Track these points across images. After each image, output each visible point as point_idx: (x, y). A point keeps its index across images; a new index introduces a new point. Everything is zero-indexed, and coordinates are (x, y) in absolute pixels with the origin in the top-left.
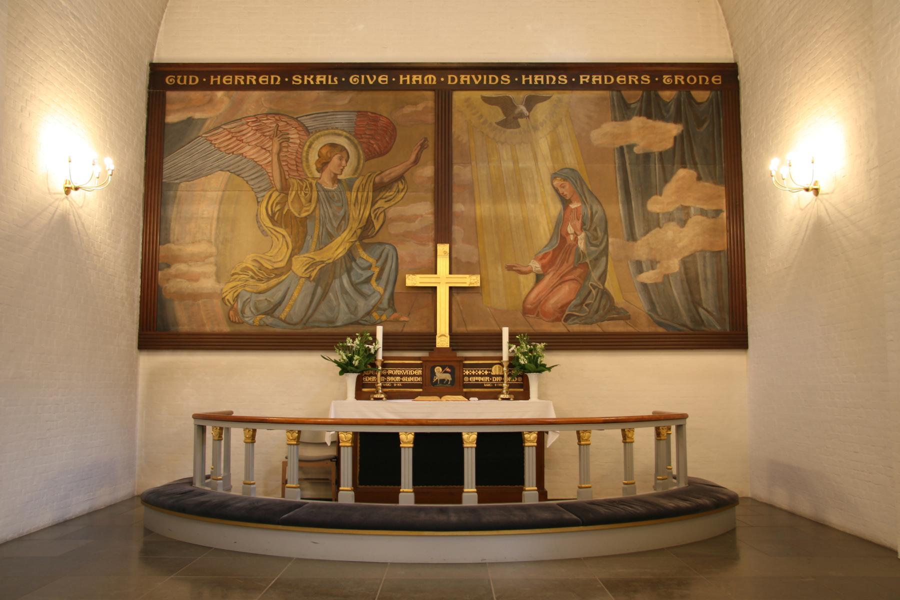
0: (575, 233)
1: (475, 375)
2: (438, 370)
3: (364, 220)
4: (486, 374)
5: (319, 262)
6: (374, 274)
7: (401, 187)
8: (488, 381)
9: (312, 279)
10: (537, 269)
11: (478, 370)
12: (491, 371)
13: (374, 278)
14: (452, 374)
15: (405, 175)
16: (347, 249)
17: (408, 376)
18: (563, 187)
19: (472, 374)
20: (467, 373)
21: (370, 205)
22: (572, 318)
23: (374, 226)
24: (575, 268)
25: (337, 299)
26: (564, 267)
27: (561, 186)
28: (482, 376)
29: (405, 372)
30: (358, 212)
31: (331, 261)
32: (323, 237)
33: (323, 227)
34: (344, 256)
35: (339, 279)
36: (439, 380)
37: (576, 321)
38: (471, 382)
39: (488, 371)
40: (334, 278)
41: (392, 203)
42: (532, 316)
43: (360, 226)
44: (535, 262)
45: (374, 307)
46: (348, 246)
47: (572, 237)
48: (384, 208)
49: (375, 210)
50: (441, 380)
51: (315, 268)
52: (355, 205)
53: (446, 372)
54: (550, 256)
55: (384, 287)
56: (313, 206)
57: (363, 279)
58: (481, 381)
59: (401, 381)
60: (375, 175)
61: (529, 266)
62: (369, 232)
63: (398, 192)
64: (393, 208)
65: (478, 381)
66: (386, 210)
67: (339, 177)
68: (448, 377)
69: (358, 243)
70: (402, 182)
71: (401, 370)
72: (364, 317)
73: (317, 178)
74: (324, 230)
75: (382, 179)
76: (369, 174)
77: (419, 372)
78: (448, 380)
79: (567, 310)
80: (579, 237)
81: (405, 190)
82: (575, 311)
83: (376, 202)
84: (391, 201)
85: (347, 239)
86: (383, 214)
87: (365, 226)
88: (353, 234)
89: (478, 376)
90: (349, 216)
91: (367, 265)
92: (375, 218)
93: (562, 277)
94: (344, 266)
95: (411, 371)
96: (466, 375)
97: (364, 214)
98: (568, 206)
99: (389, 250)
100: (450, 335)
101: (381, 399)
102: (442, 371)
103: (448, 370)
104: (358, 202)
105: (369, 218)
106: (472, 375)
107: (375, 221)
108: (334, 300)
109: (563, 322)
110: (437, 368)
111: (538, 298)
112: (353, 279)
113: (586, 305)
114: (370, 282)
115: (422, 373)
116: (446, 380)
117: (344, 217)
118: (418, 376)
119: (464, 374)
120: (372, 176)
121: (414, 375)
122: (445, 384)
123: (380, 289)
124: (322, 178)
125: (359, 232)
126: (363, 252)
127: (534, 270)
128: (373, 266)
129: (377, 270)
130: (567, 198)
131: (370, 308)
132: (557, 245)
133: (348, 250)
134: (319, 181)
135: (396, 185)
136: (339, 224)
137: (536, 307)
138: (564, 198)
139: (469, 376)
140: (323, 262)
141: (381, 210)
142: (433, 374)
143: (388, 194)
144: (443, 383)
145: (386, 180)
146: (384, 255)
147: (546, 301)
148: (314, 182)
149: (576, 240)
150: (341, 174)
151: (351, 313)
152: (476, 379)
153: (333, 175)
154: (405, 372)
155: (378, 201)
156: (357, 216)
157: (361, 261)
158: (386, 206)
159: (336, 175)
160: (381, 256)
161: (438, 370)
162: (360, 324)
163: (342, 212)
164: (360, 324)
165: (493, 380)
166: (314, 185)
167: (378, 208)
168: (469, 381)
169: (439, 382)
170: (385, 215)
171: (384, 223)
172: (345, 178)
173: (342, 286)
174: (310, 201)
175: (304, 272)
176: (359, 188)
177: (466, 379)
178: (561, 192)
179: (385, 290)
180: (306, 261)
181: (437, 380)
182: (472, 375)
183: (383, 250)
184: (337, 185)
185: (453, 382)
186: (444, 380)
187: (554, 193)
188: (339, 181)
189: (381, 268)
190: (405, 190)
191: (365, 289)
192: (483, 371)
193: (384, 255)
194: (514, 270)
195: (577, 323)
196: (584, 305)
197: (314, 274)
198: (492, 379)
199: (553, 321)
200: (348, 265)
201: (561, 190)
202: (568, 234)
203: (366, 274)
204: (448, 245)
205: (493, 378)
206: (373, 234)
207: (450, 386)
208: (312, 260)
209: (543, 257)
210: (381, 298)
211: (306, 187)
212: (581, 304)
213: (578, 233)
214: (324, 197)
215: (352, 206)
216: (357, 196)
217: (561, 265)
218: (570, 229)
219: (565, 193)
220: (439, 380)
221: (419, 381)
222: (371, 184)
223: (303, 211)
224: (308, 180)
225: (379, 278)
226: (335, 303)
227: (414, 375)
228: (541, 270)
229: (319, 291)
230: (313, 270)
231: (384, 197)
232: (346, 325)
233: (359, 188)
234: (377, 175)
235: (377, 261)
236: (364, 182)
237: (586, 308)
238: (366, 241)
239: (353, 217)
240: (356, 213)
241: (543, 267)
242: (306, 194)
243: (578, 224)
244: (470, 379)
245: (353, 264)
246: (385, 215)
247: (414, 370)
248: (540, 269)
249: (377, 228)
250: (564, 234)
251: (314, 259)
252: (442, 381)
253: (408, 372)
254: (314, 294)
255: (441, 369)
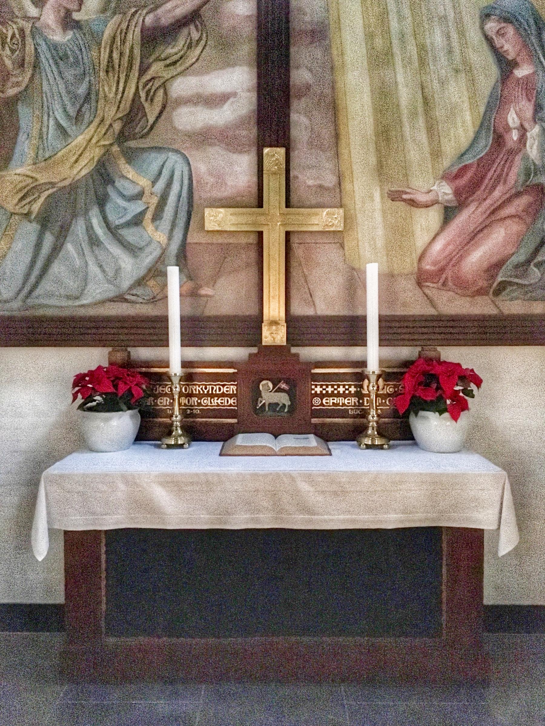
0: (522, 125)
1: (332, 395)
2: (266, 385)
3: (126, 105)
4: (353, 392)
5: (45, 184)
6: (148, 208)
7: (195, 35)
8: (355, 406)
9: (33, 217)
10: (446, 197)
11: (339, 386)
12: (361, 387)
13: (149, 215)
14: (291, 393)
15: (202, 12)
16: (96, 159)
17: (212, 396)
18: (503, 35)
19: (327, 392)
20: (318, 390)
21: (137, 74)
22: (509, 289)
23: (145, 115)
24: (518, 194)
25: (82, 254)
26: (497, 193)
27: (498, 32)
28: (344, 395)
29: (206, 388)
30: (114, 89)
31: (67, 183)
32: (50, 136)
33: (49, 116)
34: (90, 174)
35: (82, 219)
36: (267, 404)
37: (514, 295)
38: (324, 406)
39: (356, 386)
40: (74, 216)
41: (179, 68)
42: (435, 285)
43: (120, 115)
44: (444, 183)
45: (150, 270)
46: (97, 153)
47: (515, 135)
48: (164, 80)
49: (146, 84)
50: (270, 404)
51: (39, 197)
52: (107, 72)
53: (280, 390)
54: (469, 174)
55: (167, 231)
56: (29, 74)
57: (128, 217)
58: (344, 405)
59: (199, 404)
60: (145, 12)
61: (431, 191)
62: (137, 126)
63: (190, 47)
64: (179, 80)
65: (338, 405)
66: (168, 85)
67: (76, 16)
68: (283, 399)
69: (115, 149)
70: (196, 27)
71: (199, 386)
72: (130, 288)
73: (35, 18)
74: (52, 122)
75: (158, 19)
76: (133, 10)
77: (232, 389)
78: (284, 405)
79: (500, 274)
80: (528, 134)
81: (204, 39)
82: (516, 277)
83: (149, 67)
84: (178, 64)
85: (94, 141)
86: (161, 92)
87: (128, 114)
88: (107, 130)
89: (339, 395)
90: (97, 95)
91: (135, 190)
92: (146, 100)
93: (493, 212)
94: (92, 192)
95: (218, 387)
96: (316, 395)
97: (126, 92)
98: (512, 73)
99: (176, 162)
100: (287, 321)
101: (181, 446)
102: (273, 389)
103: (283, 386)
104: (113, 67)
105: (137, 99)
106: (328, 395)
107: (146, 105)
108: (76, 255)
109: (491, 296)
110: (264, 382)
111: (447, 252)
112: (112, 217)
113: (536, 265)
114: (142, 222)
115: (236, 390)
116: (281, 405)
117: (87, 98)
118: (230, 396)
119: (313, 392)
120: (140, 12)
121: (223, 395)
122: (278, 412)
123: (161, 237)
124: (42, 18)
125: (117, 126)
126: (127, 165)
127: (440, 199)
128: (147, 192)
129: (155, 200)
130: (510, 58)
131: (142, 272)
132: (488, 148)
133: (99, 161)
134: (37, 25)
135: (185, 31)
136: (79, 111)
137: (442, 270)
138: (502, 56)
139: (322, 396)
140: (53, 184)
141: (157, 83)
142: (258, 394)
143: (170, 50)
144: (275, 411)
145: (165, 21)
146: (166, 173)
147: (461, 258)
148: (28, 26)
149: (523, 139)
150: (79, 10)
151: (109, 282)
152: (335, 401)
153: (62, 14)
154: (206, 388)
155: (151, 63)
156: (112, 95)
157: (126, 184)
158: (166, 75)
159: (68, 13)
160: (160, 173)
161: (266, 385)
162: (126, 301)
163: (82, 90)
164: (126, 301)
165: (365, 404)
166: (28, 32)
167: (153, 78)
168: (322, 404)
169: (267, 409)
170: (166, 93)
171: (164, 107)
172: (86, 18)
173: (89, 228)
174: (22, 65)
175: (17, 205)
176: (114, 38)
177: (317, 401)
178: (498, 46)
179: (170, 238)
180: (21, 182)
181: (264, 404)
182: (328, 395)
183: (164, 163)
184: (72, 33)
185: (292, 409)
186: (277, 404)
187: (485, 46)
188: (77, 25)
189: (162, 196)
190: (203, 43)
191: (130, 235)
192: (336, 387)
193: (166, 173)
194: (404, 200)
195: (517, 298)
196: (532, 264)
197: (36, 207)
198: (363, 402)
199: (473, 296)
200: (101, 191)
201: (498, 42)
202: (508, 129)
203: (136, 208)
204: (207, 211)
205: (365, 399)
206: (146, 130)
207: (286, 415)
208: (30, 180)
209: (458, 176)
210: (162, 254)
211: (13, 36)
212: (528, 262)
213: (527, 125)
214: (49, 56)
215: (102, 74)
216: (111, 57)
217: (494, 188)
218: (512, 119)
219: (506, 47)
220: (267, 404)
221: (231, 405)
222: (138, 30)
223: (10, 84)
224: (15, 23)
225: (157, 216)
226: (78, 262)
227: (223, 395)
228: (454, 199)
229: (49, 240)
230: (35, 200)
231: (163, 56)
232: (103, 302)
233: (114, 38)
234: (147, 13)
235: (154, 183)
236: (124, 26)
237: (535, 269)
238: (132, 144)
239: (106, 96)
240: (110, 89)
241: (457, 193)
242: (13, 51)
243: (528, 109)
244: (324, 401)
245: (110, 189)
246: (166, 93)
247: (223, 386)
248: (451, 197)
249: (151, 120)
250: (501, 130)
251: (36, 180)
252: (273, 406)
253: (212, 388)
254: (38, 245)
255: (271, 385)
